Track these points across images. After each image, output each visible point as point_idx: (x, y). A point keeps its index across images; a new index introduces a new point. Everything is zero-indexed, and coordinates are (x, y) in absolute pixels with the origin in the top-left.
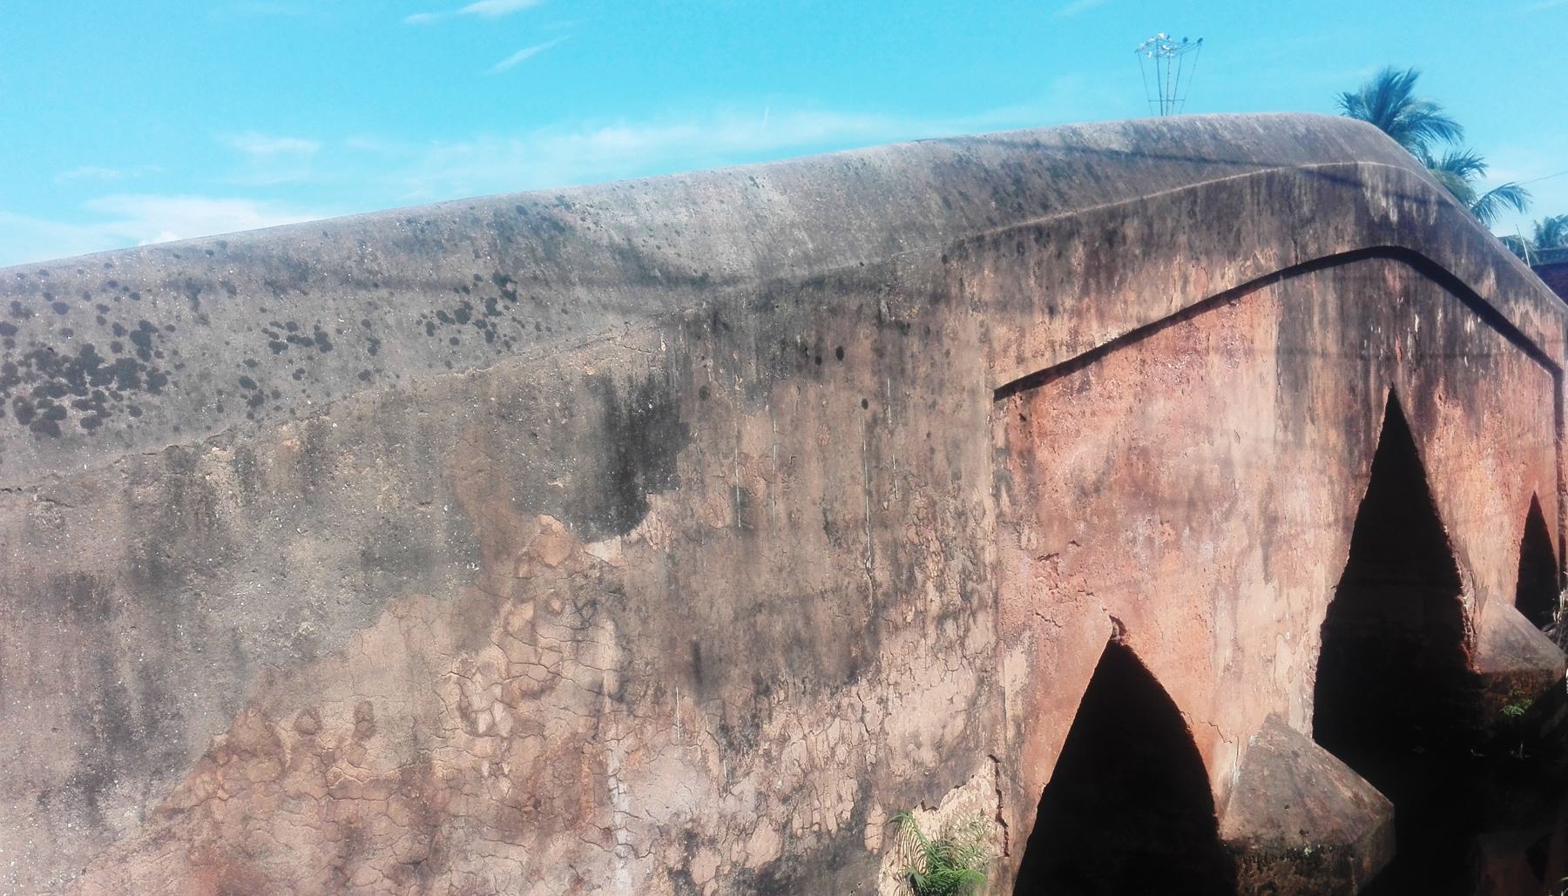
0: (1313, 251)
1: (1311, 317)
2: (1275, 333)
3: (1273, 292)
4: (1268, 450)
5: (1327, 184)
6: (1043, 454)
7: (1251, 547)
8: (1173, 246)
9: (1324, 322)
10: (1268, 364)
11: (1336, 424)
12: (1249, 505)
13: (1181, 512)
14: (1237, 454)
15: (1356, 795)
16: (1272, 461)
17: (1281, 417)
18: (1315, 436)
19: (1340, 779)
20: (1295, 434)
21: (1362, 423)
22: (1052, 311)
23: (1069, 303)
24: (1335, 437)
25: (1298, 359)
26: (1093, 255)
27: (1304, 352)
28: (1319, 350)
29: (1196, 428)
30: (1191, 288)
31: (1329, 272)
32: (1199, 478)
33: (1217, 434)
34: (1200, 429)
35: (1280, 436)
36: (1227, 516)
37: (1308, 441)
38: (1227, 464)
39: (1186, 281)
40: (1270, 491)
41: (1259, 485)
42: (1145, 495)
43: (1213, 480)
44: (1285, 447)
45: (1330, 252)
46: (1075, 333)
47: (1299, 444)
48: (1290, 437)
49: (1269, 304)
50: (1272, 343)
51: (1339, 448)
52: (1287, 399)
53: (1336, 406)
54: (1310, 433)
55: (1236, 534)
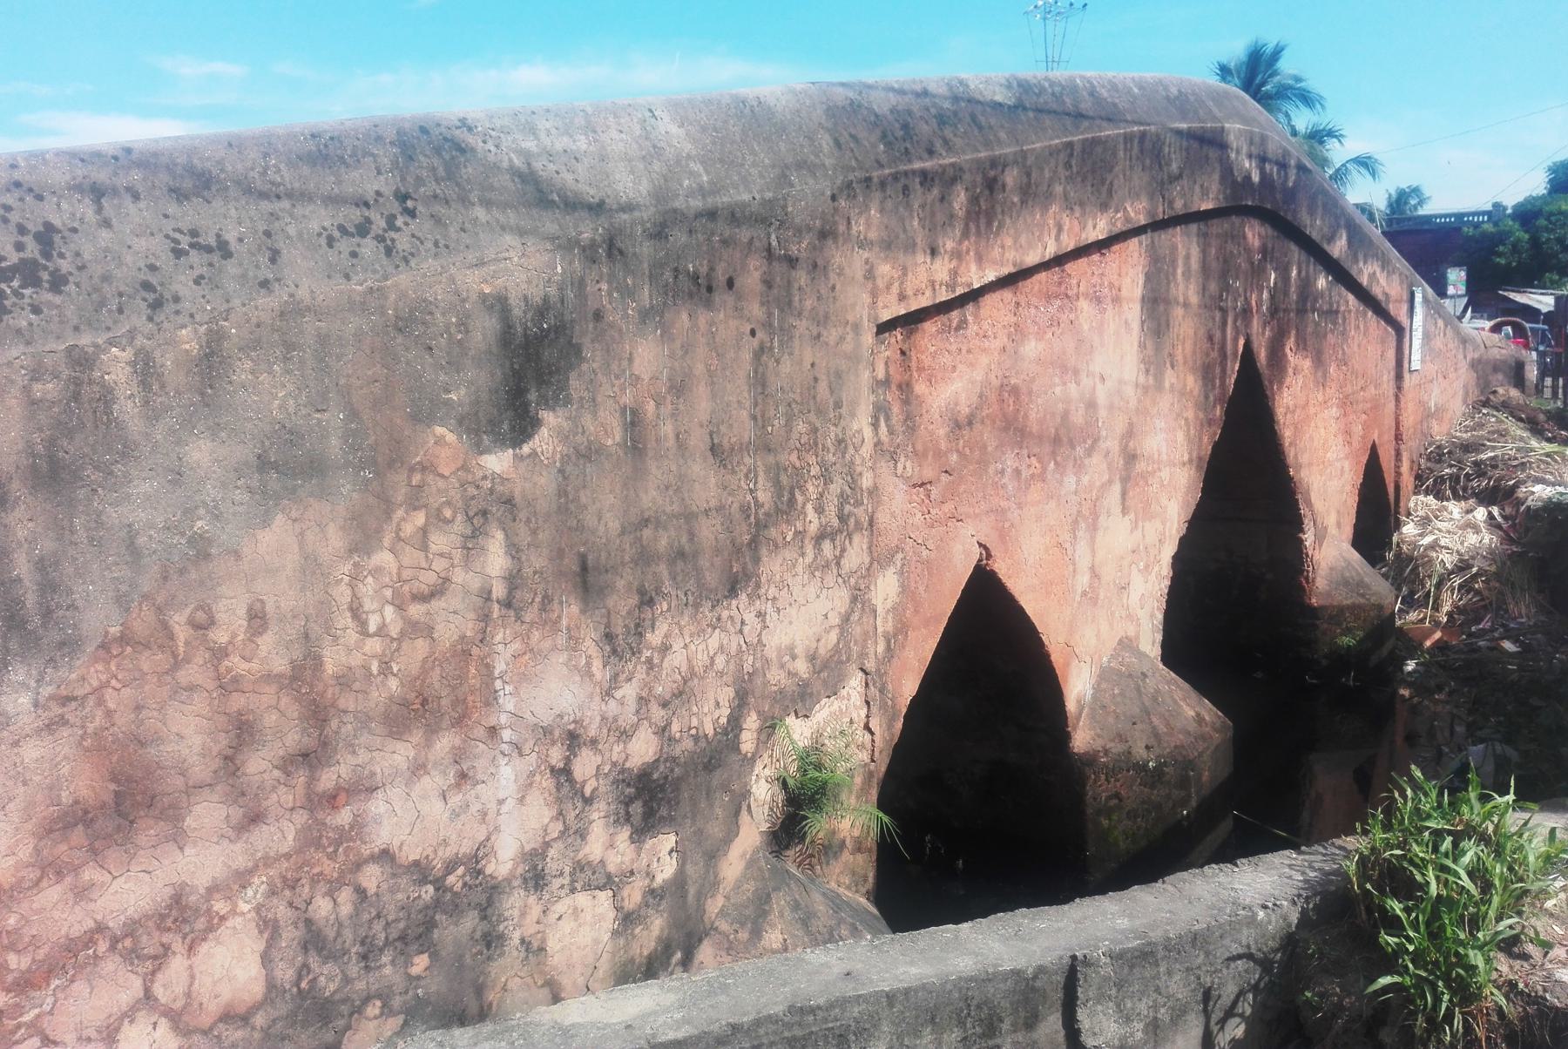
0: (1179, 206)
1: (1175, 270)
2: (1141, 282)
3: (1141, 243)
4: (1130, 391)
5: (1195, 145)
6: (920, 388)
7: (1110, 482)
8: (1049, 197)
9: (1187, 274)
10: (1133, 312)
11: (1193, 370)
12: (1111, 444)
13: (1047, 448)
14: (1102, 397)
15: (1198, 715)
16: (1133, 404)
17: (1143, 361)
18: (1174, 380)
19: (1184, 700)
20: (1155, 376)
21: (1218, 370)
22: (934, 252)
23: (950, 245)
24: (1192, 383)
25: (1162, 308)
26: (974, 200)
27: (1167, 302)
28: (1181, 300)
29: (1064, 369)
30: (1064, 237)
31: (1194, 227)
32: (1065, 415)
33: (1083, 376)
34: (1068, 370)
35: (1142, 379)
36: (1089, 452)
37: (1167, 385)
38: (1091, 405)
39: (1060, 229)
40: (1130, 433)
41: (1120, 426)
42: (1014, 429)
43: (1078, 418)
44: (1146, 389)
45: (1194, 209)
46: (954, 273)
47: (1159, 387)
48: (1151, 381)
49: (1136, 255)
50: (1138, 292)
51: (1196, 392)
52: (1149, 344)
53: (1194, 352)
54: (1170, 377)
55: (1097, 469)
